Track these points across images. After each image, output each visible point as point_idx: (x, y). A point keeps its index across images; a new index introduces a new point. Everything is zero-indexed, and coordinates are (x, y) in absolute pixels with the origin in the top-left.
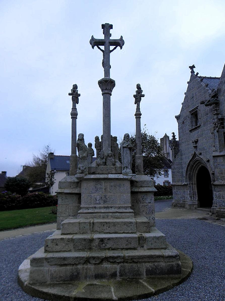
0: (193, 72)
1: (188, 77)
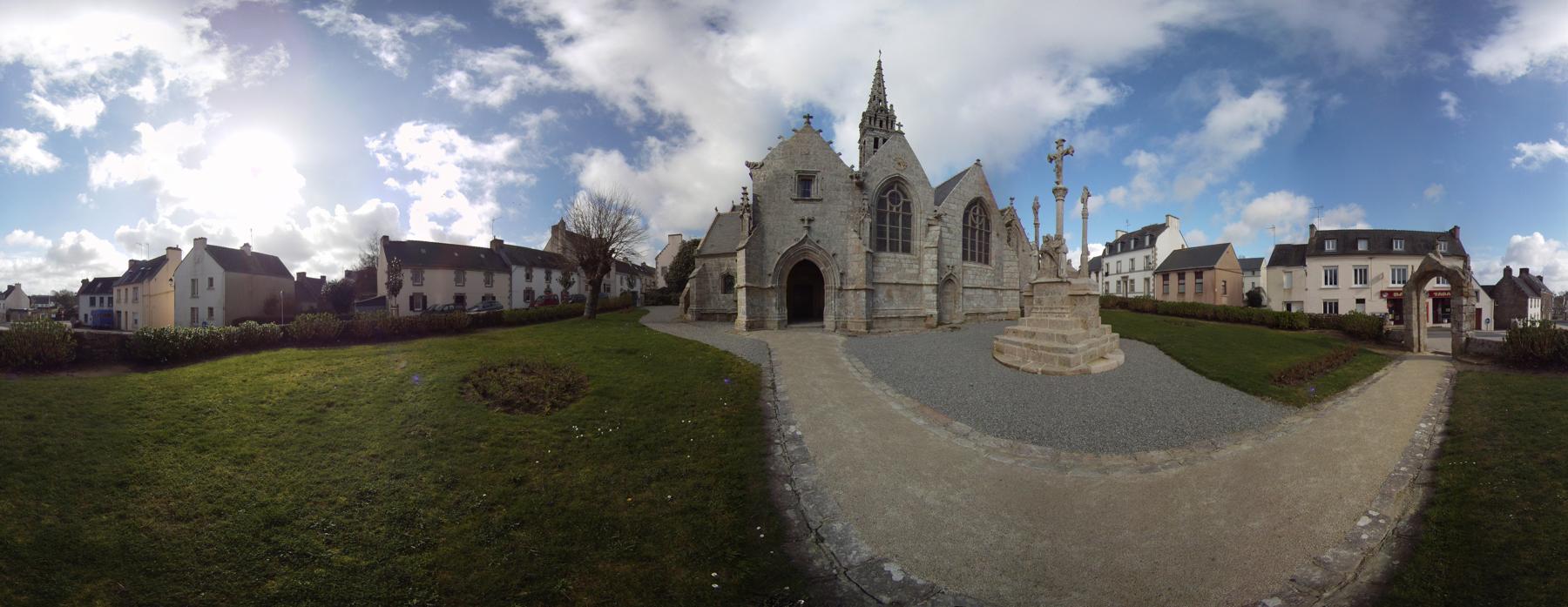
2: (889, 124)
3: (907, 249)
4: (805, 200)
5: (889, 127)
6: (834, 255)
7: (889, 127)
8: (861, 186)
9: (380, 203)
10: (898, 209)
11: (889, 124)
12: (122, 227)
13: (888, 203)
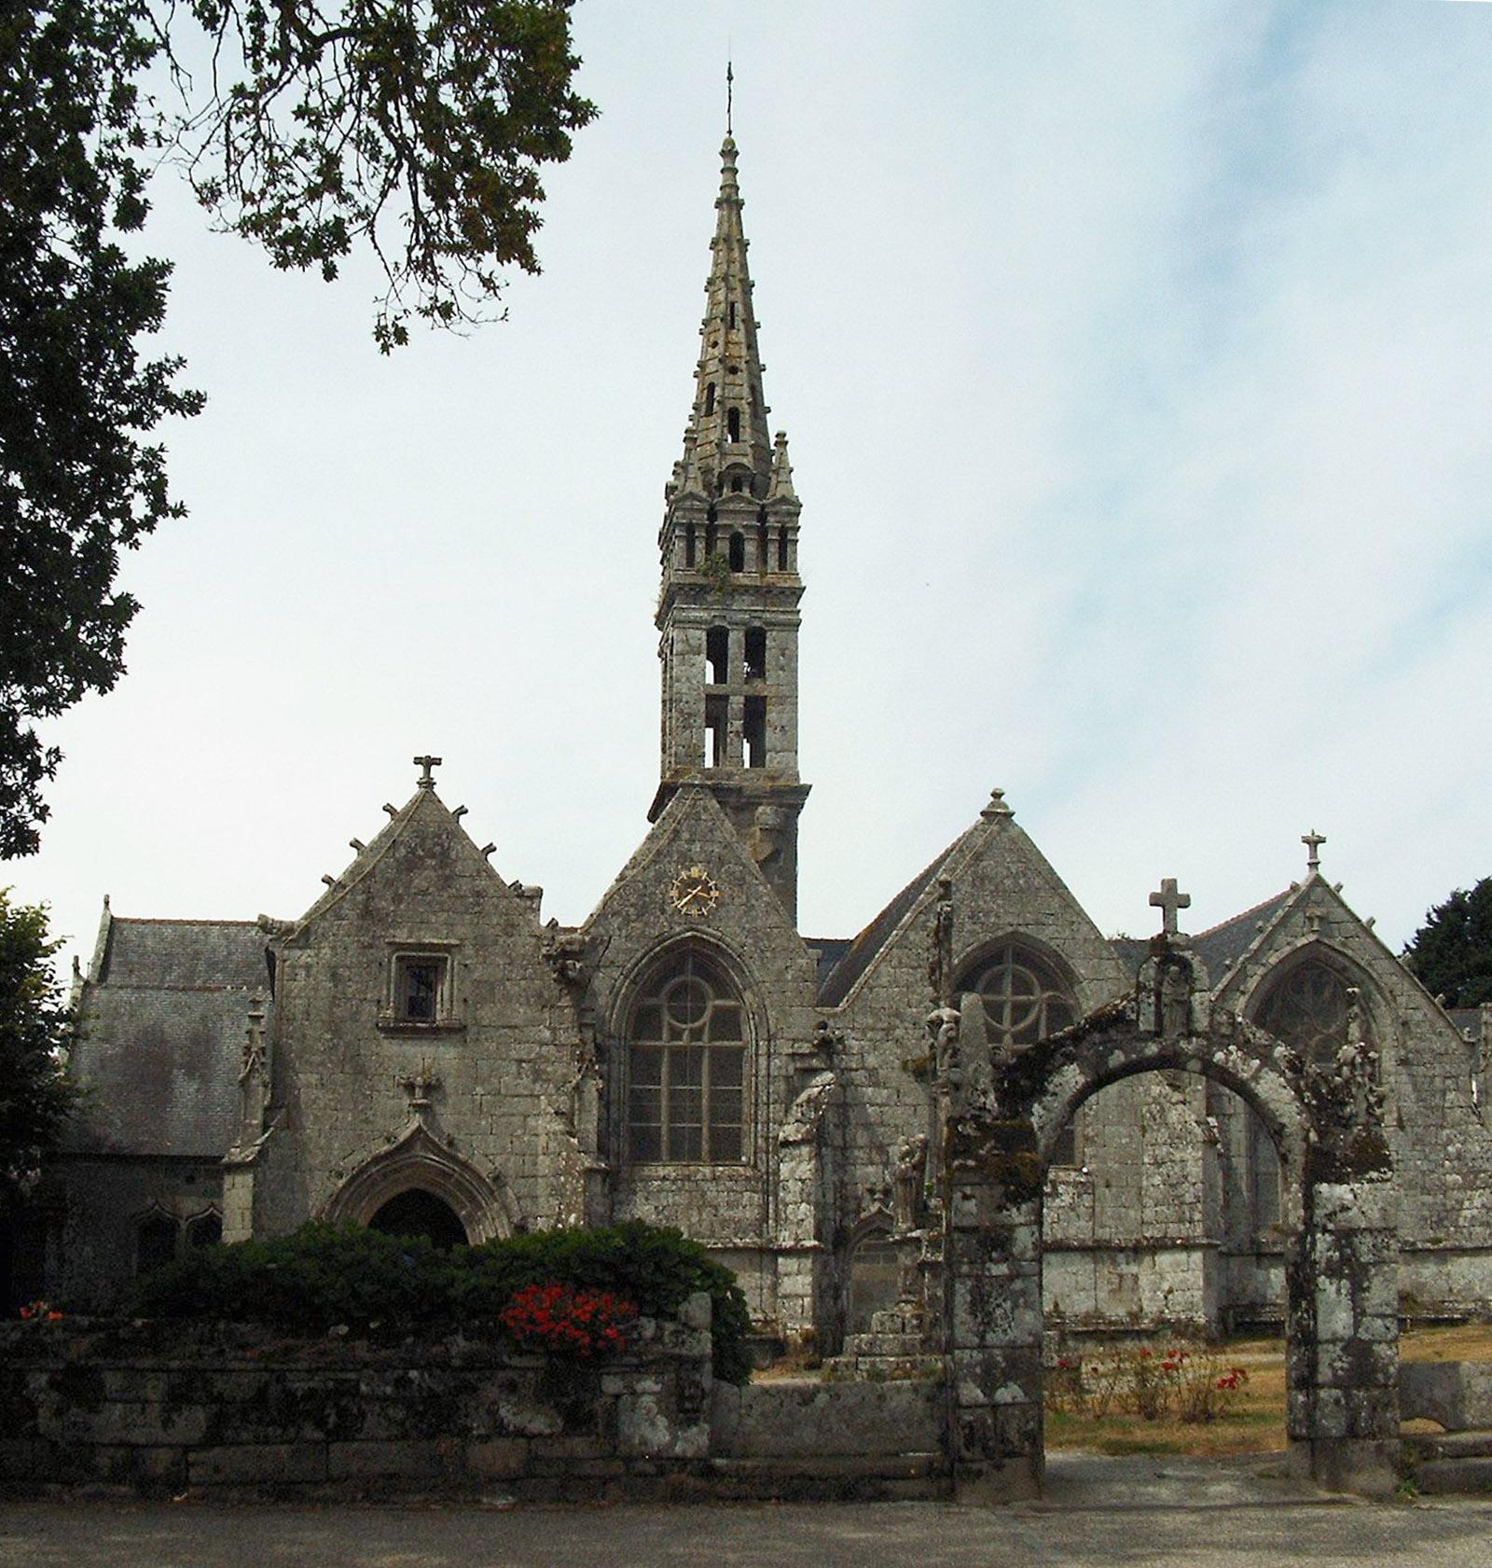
0: (427, 784)
1: (404, 793)
2: (773, 548)
3: (726, 1148)
4: (416, 1031)
5: (773, 562)
6: (496, 1179)
7: (773, 562)
8: (577, 987)
9: (298, 223)
10: (696, 1034)
11: (773, 548)
12: (390, 113)
13: (667, 1018)
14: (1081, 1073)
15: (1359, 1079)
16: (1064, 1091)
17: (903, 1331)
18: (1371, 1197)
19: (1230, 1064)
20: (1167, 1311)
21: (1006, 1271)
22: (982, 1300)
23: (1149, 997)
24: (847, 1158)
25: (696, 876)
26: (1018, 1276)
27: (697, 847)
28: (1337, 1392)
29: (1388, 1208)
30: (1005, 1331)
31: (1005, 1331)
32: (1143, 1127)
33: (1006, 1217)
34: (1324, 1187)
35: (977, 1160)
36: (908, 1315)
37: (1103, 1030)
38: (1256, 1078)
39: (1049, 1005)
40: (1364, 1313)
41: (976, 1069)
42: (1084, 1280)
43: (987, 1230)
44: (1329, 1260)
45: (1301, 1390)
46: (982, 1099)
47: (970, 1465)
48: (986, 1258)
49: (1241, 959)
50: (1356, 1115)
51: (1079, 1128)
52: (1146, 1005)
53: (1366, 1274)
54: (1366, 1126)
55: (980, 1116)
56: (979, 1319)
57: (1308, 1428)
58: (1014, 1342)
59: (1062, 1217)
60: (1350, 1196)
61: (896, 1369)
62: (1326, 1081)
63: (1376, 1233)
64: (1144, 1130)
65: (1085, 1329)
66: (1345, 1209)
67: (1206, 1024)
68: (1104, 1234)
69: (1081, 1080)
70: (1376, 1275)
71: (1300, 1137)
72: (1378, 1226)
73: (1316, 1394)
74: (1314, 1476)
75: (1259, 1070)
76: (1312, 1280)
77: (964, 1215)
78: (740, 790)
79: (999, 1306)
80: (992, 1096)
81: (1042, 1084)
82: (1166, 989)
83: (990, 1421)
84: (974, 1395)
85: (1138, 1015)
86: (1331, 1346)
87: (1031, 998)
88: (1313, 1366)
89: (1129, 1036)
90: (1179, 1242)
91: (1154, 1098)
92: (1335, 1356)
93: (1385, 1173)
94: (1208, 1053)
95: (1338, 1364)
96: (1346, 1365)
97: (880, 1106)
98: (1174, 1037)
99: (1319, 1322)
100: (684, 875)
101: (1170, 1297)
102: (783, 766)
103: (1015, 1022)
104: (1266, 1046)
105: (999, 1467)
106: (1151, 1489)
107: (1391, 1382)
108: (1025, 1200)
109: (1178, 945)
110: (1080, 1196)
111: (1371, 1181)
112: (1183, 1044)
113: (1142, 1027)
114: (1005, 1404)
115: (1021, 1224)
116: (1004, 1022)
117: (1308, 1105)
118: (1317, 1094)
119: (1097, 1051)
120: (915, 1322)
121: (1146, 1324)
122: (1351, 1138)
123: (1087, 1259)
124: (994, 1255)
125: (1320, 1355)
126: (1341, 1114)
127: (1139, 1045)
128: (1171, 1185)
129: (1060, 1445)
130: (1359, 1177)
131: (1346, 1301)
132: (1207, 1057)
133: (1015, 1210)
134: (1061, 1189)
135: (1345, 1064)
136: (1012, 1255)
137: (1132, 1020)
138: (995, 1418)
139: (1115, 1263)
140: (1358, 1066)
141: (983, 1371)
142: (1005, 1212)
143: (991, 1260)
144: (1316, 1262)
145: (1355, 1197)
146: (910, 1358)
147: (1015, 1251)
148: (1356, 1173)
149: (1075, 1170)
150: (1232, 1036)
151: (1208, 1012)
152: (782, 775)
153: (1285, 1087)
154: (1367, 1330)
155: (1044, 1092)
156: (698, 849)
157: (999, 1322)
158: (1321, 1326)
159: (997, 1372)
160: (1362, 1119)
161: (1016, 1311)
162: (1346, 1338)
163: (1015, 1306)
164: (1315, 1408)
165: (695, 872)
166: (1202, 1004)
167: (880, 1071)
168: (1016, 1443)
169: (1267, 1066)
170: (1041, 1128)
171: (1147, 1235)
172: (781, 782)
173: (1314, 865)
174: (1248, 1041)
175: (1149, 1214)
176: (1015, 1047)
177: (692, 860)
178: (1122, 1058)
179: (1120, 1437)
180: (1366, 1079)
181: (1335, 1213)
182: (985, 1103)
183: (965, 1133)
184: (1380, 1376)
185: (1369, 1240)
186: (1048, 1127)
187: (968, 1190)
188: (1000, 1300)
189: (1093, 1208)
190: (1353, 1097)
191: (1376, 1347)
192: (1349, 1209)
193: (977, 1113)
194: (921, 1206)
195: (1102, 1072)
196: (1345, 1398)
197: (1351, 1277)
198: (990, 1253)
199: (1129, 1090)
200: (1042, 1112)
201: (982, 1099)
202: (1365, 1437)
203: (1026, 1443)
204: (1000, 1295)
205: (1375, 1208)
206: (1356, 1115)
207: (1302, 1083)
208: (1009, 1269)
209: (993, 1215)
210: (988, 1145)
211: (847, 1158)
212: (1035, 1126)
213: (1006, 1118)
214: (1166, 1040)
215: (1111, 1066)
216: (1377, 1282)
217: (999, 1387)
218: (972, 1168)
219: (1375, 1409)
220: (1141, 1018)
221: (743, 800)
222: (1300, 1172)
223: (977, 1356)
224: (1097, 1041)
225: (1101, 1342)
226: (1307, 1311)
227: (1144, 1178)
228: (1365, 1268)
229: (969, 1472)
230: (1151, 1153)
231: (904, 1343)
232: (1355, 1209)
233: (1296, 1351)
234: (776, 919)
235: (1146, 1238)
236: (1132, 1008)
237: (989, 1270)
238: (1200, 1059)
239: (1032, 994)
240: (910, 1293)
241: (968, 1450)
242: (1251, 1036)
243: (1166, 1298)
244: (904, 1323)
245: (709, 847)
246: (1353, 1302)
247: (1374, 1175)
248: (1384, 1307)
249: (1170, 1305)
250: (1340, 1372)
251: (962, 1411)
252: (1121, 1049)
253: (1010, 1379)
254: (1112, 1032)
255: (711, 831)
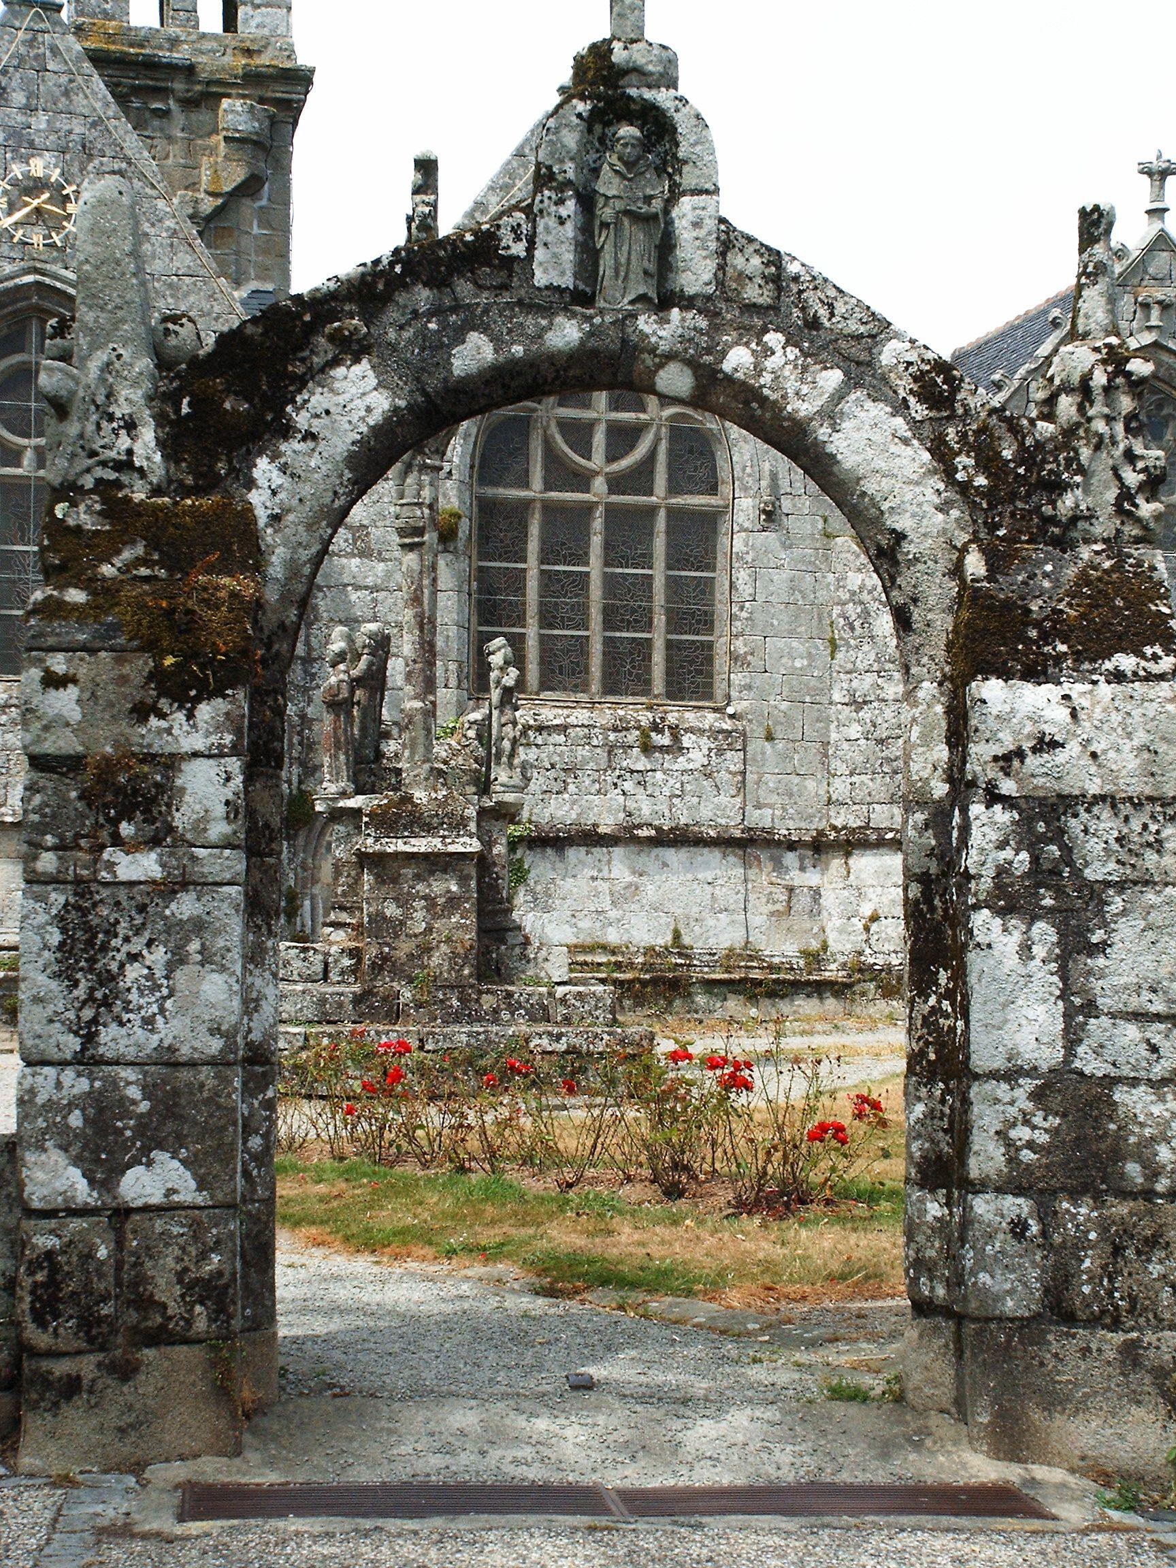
14: (380, 385)
15: (1100, 426)
16: (334, 431)
17: (325, 977)
18: (1116, 718)
19: (766, 379)
20: (868, 951)
21: (157, 872)
22: (90, 943)
23: (560, 202)
24: (313, 676)
25: (40, 174)
26: (184, 885)
27: (40, 121)
28: (1017, 1205)
29: (1162, 747)
30: (148, 1022)
31: (148, 1022)
32: (832, 642)
33: (160, 731)
34: (991, 690)
35: (93, 593)
36: (334, 949)
37: (439, 283)
38: (831, 414)
39: (672, 428)
40: (1090, 1008)
41: (107, 367)
42: (729, 893)
43: (108, 767)
44: (1002, 871)
45: (932, 1191)
46: (124, 442)
47: (45, 1365)
48: (104, 835)
49: (1022, 371)
50: (1090, 517)
51: (723, 640)
52: (552, 222)
53: (1100, 913)
54: (1113, 543)
55: (118, 484)
56: (81, 992)
57: (948, 1285)
58: (172, 1049)
59: (688, 787)
60: (1063, 714)
61: (302, 1048)
62: (1013, 427)
63: (1126, 809)
64: (834, 646)
65: (726, 976)
66: (1046, 744)
67: (707, 276)
68: (761, 818)
69: (381, 403)
70: (1124, 913)
71: (941, 567)
72: (1133, 791)
73: (968, 1208)
74: (960, 1409)
75: (839, 396)
76: (959, 919)
77: (46, 728)
78: (189, 70)
79: (134, 957)
80: (148, 434)
81: (281, 413)
82: (609, 185)
83: (102, 1253)
84: (60, 1185)
85: (530, 249)
86: (1005, 1086)
87: (642, 416)
88: (960, 1131)
89: (506, 298)
90: (890, 836)
91: (853, 593)
92: (1012, 1111)
93: (1155, 658)
94: (708, 351)
95: (1021, 1133)
96: (1042, 1138)
97: (375, 589)
98: (625, 303)
99: (974, 1024)
100: (17, 170)
101: (874, 927)
102: (266, 32)
103: (611, 458)
104: (859, 337)
105: (125, 1371)
106: (542, 1424)
107: (1162, 1185)
108: (207, 694)
109: (637, 70)
110: (720, 752)
111: (1118, 677)
112: (646, 323)
113: (541, 278)
114: (146, 1209)
115: (196, 755)
116: (594, 456)
117: (964, 488)
118: (988, 460)
119: (423, 333)
120: (347, 962)
121: (832, 972)
122: (1071, 572)
123: (732, 859)
124: (126, 829)
125: (976, 1109)
126: (1047, 510)
127: (531, 322)
128: (880, 742)
129: (451, 1253)
130: (1086, 666)
131: (1045, 978)
132: (708, 359)
133: (180, 716)
134: (687, 740)
135: (1065, 388)
136: (171, 829)
137: (515, 258)
138: (120, 1244)
139: (778, 866)
140: (1099, 399)
141: (86, 1120)
142: (154, 722)
143: (117, 841)
144: (967, 876)
145: (1074, 714)
146: (330, 1029)
147: (180, 820)
148: (1078, 657)
149: (715, 710)
150: (774, 308)
151: (713, 245)
152: (265, 47)
153: (906, 442)
154: (1098, 1051)
155: (286, 431)
156: (43, 126)
157: (134, 996)
158: (978, 1038)
159: (127, 1126)
160: (1104, 526)
161: (179, 975)
162: (1044, 1067)
163: (178, 960)
164: (963, 1240)
165: (38, 167)
166: (697, 225)
167: (372, 530)
168: (173, 1309)
169: (857, 385)
170: (275, 519)
171: (838, 823)
172: (264, 60)
173: (1157, 213)
174: (814, 324)
175: (840, 788)
176: (615, 498)
177: (32, 145)
178: (488, 353)
179: (580, 1241)
180: (1119, 428)
181: (1020, 754)
182: (130, 452)
183: (71, 522)
184: (1133, 1169)
185: (1107, 824)
186: (291, 517)
187: (59, 663)
188: (137, 945)
189: (743, 773)
190: (1081, 470)
191: (1128, 1098)
192: (1054, 745)
193: (111, 475)
194: (369, 753)
195: (433, 383)
196: (1041, 1220)
197: (1062, 917)
198: (115, 822)
199: (809, 578)
200: (278, 479)
201: (124, 442)
202: (1093, 1322)
203: (198, 1309)
204: (138, 931)
205: (1127, 746)
206: (1090, 517)
207: (951, 434)
208: (163, 865)
209: (124, 726)
210: (127, 555)
211: (313, 676)
212: (262, 515)
213: (187, 492)
214: (601, 312)
215: (456, 372)
216: (1126, 932)
217: (129, 1166)
218: (75, 607)
219: (1117, 1251)
220: (539, 254)
221: (198, 88)
222: (941, 654)
223: (76, 1084)
224: (423, 308)
225: (753, 999)
226: (949, 995)
227: (833, 726)
228: (1095, 894)
229: (45, 1381)
230: (845, 685)
231: (323, 1001)
232: (1073, 748)
233: (923, 1091)
234: (188, 260)
235: (834, 828)
236: (515, 230)
237: (110, 866)
238: (692, 364)
239: (644, 411)
240: (342, 908)
241: (42, 1324)
242: (823, 312)
243: (867, 929)
244: (326, 964)
245: (63, 124)
246: (1064, 978)
247: (1126, 662)
248: (1146, 995)
249: (873, 941)
250: (1027, 1156)
251: (29, 1224)
252: (485, 329)
253: (161, 1146)
254: (464, 288)
255: (66, 93)
